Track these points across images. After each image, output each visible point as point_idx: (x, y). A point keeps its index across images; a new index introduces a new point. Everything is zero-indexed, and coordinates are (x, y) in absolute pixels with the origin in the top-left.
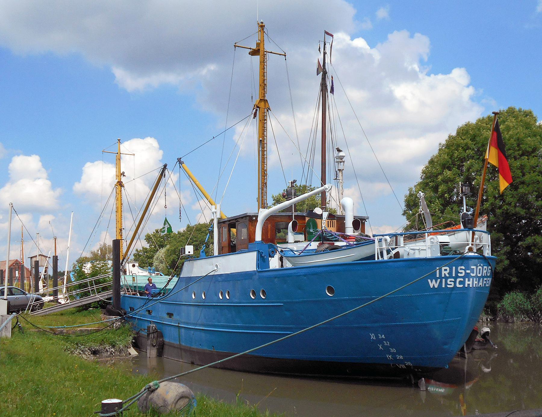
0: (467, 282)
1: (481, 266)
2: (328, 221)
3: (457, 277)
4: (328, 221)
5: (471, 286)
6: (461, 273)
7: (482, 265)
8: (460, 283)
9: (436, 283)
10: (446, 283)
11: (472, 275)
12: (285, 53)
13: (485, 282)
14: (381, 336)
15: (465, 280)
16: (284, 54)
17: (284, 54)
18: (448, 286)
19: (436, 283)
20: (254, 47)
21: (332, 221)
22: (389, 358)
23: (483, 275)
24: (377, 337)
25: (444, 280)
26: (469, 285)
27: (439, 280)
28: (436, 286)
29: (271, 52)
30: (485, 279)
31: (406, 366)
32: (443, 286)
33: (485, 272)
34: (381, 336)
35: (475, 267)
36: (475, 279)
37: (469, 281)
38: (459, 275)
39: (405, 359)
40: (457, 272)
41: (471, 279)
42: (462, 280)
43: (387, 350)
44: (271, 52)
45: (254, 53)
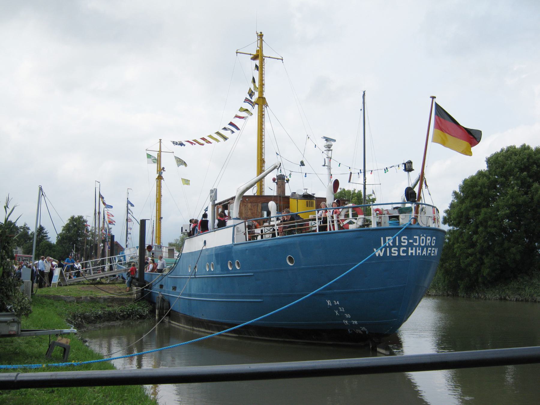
0: (410, 251)
1: (424, 236)
2: (307, 202)
3: (400, 246)
4: (307, 202)
5: (414, 254)
6: (405, 242)
7: (425, 235)
8: (404, 251)
9: (381, 252)
10: (391, 252)
11: (415, 244)
12: (282, 58)
13: (429, 252)
14: (336, 302)
15: (408, 249)
16: (281, 58)
17: (281, 58)
18: (393, 255)
19: (381, 252)
20: (255, 53)
21: (311, 202)
22: (346, 323)
23: (427, 245)
24: (333, 303)
25: (388, 249)
26: (412, 253)
27: (384, 249)
28: (381, 255)
29: (269, 57)
30: (429, 249)
31: (362, 331)
32: (388, 255)
33: (428, 242)
34: (336, 302)
35: (417, 237)
36: (418, 248)
37: (412, 249)
38: (403, 244)
39: (360, 325)
40: (400, 241)
41: (414, 248)
42: (405, 249)
43: (342, 314)
44: (269, 57)
45: (255, 58)
